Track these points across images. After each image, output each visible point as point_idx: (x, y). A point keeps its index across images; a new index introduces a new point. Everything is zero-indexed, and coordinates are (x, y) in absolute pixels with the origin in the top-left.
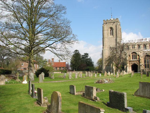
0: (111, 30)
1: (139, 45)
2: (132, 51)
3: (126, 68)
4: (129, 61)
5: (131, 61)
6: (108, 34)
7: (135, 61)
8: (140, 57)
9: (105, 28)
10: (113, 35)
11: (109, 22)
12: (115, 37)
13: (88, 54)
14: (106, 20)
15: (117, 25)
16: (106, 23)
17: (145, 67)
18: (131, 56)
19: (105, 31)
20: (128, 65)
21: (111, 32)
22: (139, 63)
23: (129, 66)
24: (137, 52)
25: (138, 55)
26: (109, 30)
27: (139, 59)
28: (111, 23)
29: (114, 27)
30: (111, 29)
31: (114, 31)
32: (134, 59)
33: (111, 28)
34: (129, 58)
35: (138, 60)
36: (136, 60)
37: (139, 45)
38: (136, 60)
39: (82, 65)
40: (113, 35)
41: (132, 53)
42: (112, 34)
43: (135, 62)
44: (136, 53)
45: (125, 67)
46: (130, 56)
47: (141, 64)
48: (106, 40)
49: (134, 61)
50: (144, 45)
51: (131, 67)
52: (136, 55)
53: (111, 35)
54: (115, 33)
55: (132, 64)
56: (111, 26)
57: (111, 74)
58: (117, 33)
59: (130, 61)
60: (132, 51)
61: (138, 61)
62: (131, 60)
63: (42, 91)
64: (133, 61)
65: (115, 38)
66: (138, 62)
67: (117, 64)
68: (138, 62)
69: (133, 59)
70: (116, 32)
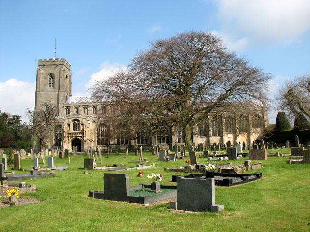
0: (50, 79)
1: (94, 107)
2: (73, 117)
3: (63, 144)
4: (68, 134)
5: (70, 133)
6: (45, 85)
7: (78, 133)
8: (84, 128)
9: (41, 74)
10: (53, 86)
11: (48, 64)
12: (57, 91)
13: (20, 117)
14: (43, 60)
15: (61, 70)
16: (44, 65)
17: (99, 144)
18: (71, 126)
19: (41, 80)
20: (66, 139)
21: (50, 82)
22: (83, 137)
23: (67, 141)
24: (80, 120)
25: (83, 125)
26: (48, 77)
27: (83, 130)
28: (52, 66)
29: (56, 73)
30: (51, 76)
31: (56, 80)
32: (76, 130)
33: (52, 75)
34: (68, 129)
35: (81, 132)
36: (79, 132)
37: (94, 107)
38: (79, 132)
39: (6, 138)
40: (53, 86)
41: (73, 121)
42: (52, 85)
43: (77, 136)
44: (79, 121)
45: (61, 143)
46: (69, 125)
47: (85, 139)
48: (41, 94)
49: (76, 133)
50: (68, 108)
51: (70, 143)
52: (79, 124)
53: (50, 87)
54: (58, 84)
55: (72, 138)
56: (51, 71)
57: (27, 155)
58: (60, 87)
59: (69, 134)
60: (73, 117)
61: (81, 133)
62: (72, 131)
63: (139, 205)
64: (74, 133)
65: (57, 93)
66: (81, 135)
67: (41, 139)
68: (81, 135)
69: (74, 129)
70: (59, 83)
